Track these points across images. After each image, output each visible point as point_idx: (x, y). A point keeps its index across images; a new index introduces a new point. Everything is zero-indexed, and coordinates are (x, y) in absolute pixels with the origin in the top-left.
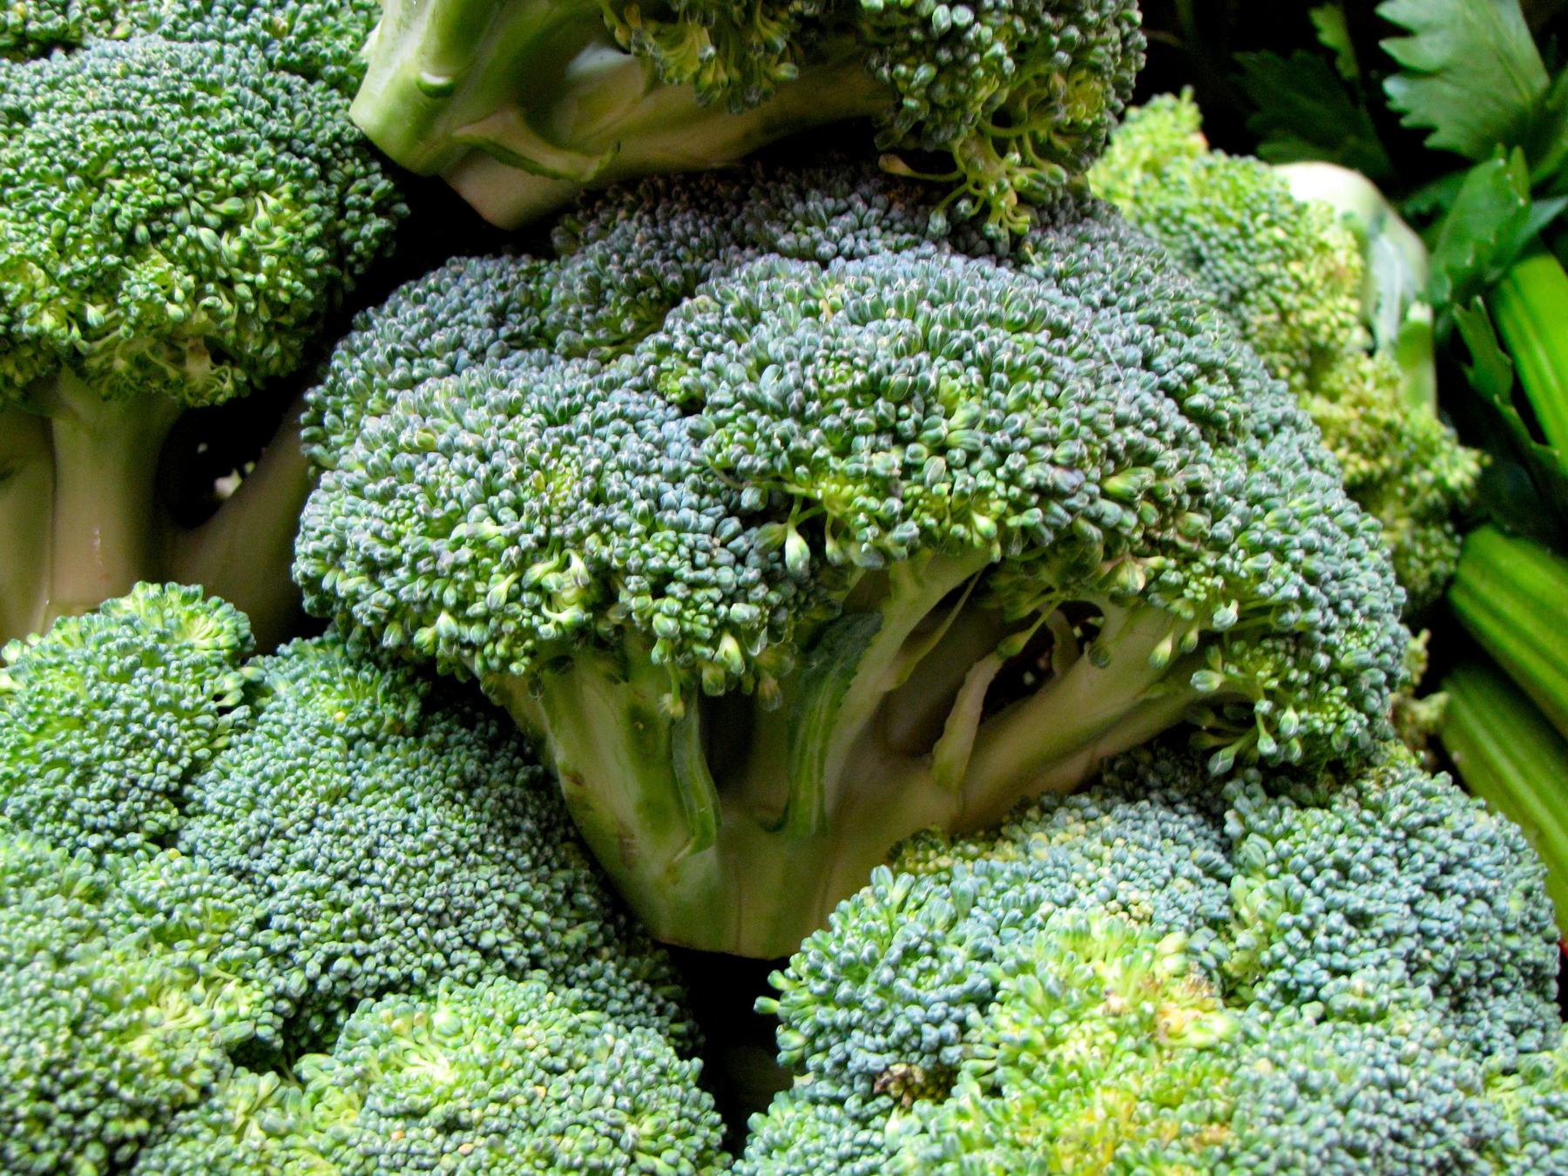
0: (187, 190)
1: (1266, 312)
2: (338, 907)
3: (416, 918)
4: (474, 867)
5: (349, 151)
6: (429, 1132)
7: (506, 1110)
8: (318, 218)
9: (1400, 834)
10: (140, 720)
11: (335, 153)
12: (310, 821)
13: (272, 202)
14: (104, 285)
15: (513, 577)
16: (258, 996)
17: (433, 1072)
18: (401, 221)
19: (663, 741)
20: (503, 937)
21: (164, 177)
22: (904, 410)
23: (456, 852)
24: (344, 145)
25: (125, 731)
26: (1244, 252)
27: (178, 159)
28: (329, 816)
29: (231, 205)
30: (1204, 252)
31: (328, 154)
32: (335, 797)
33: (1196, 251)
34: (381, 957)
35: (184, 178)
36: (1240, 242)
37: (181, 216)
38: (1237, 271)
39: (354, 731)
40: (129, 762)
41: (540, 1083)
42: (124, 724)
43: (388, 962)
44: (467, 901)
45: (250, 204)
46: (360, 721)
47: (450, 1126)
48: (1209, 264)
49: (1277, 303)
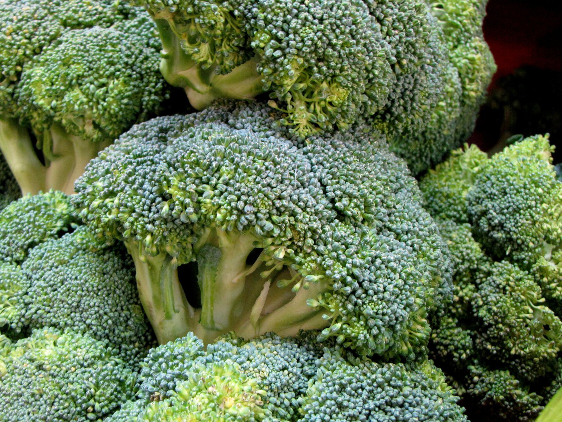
0: (90, 72)
1: (527, 220)
2: (46, 294)
3: (67, 306)
4: (93, 297)
5: (153, 74)
6: (33, 367)
7: (58, 369)
8: (130, 90)
9: (375, 384)
10: (23, 224)
11: (147, 73)
12: (51, 267)
13: (116, 82)
14: (59, 95)
15: (101, 201)
16: (16, 313)
17: (48, 353)
18: (165, 100)
19: (158, 276)
20: (93, 322)
21: (85, 67)
22: (205, 173)
23: (88, 290)
24: (151, 72)
25: (17, 226)
26: (523, 194)
27: (91, 62)
28: (57, 267)
29: (103, 80)
30: (508, 190)
31: (143, 72)
32: (62, 263)
33: (504, 189)
34: (52, 314)
35: (90, 69)
36: (523, 190)
37: (87, 80)
38: (518, 200)
39: (79, 246)
40: (15, 235)
41: (74, 366)
42: (18, 224)
43: (54, 317)
44: (86, 307)
45: (109, 81)
46: (82, 244)
47: (40, 367)
48: (508, 195)
49: (532, 217)
